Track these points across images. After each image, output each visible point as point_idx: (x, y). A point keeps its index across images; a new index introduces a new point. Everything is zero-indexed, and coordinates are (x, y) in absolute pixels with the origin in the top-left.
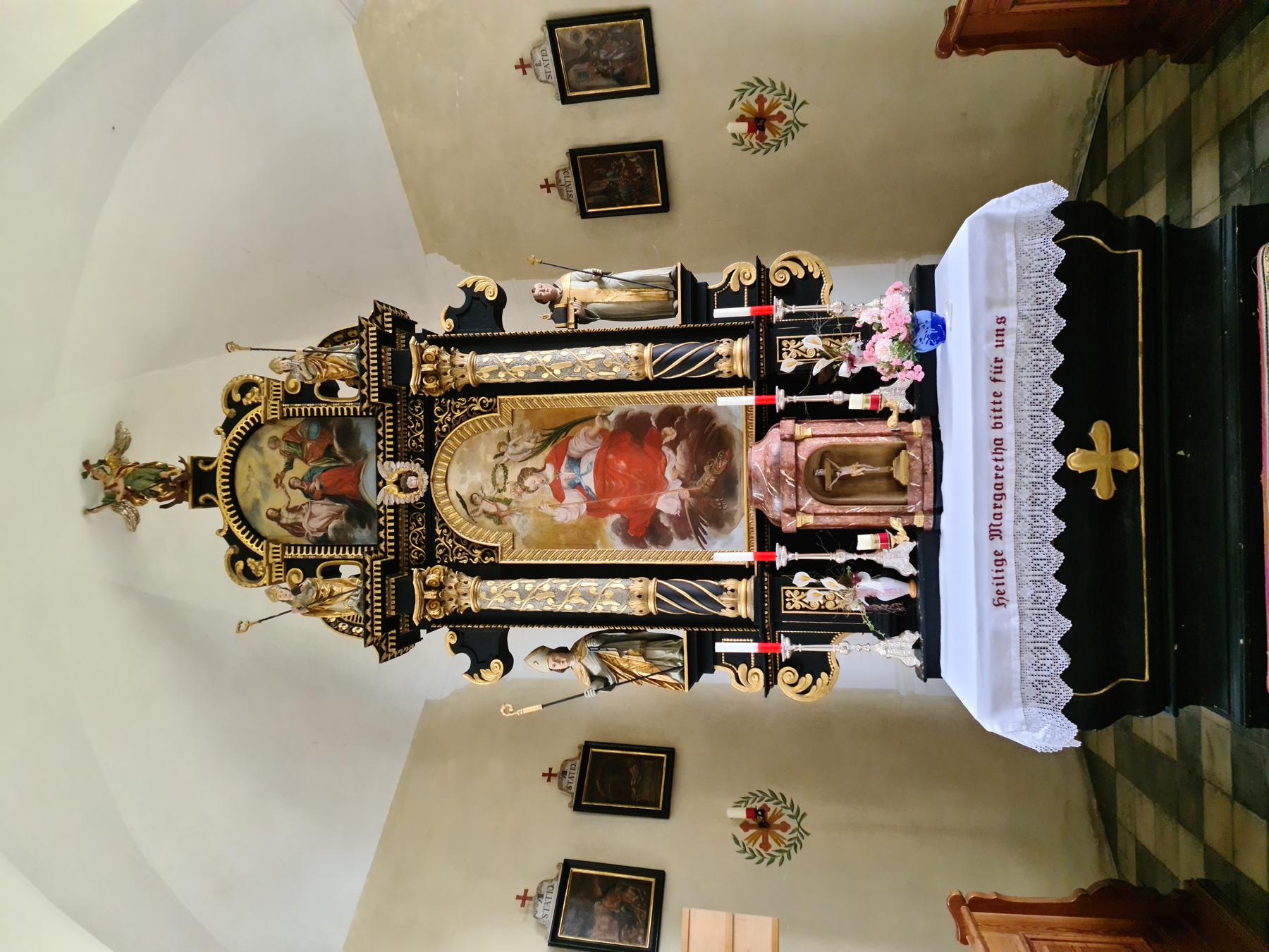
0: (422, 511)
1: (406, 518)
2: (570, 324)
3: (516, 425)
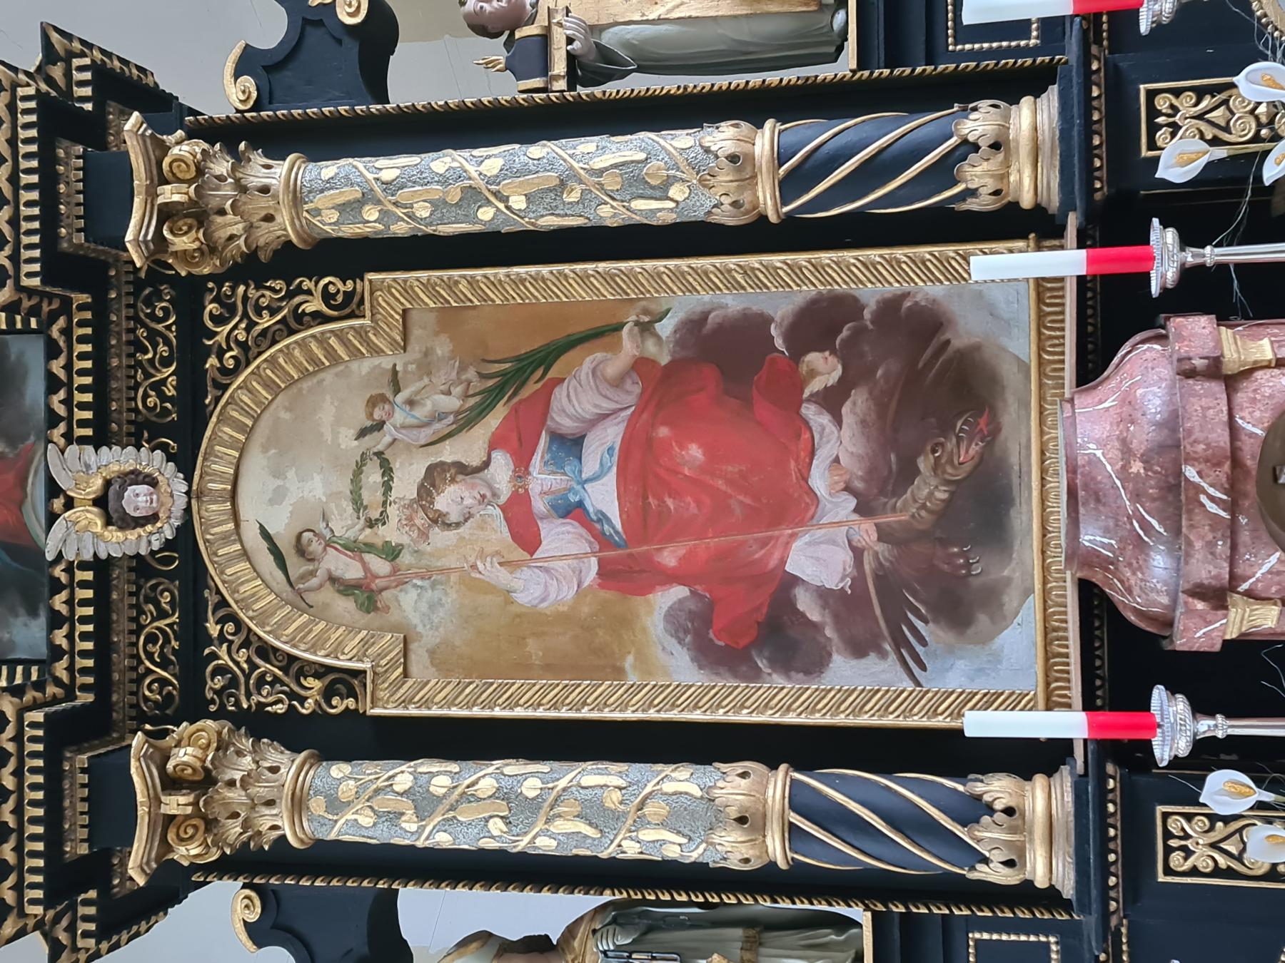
0: (170, 576)
1: (131, 594)
2: (557, 77)
3: (415, 349)
